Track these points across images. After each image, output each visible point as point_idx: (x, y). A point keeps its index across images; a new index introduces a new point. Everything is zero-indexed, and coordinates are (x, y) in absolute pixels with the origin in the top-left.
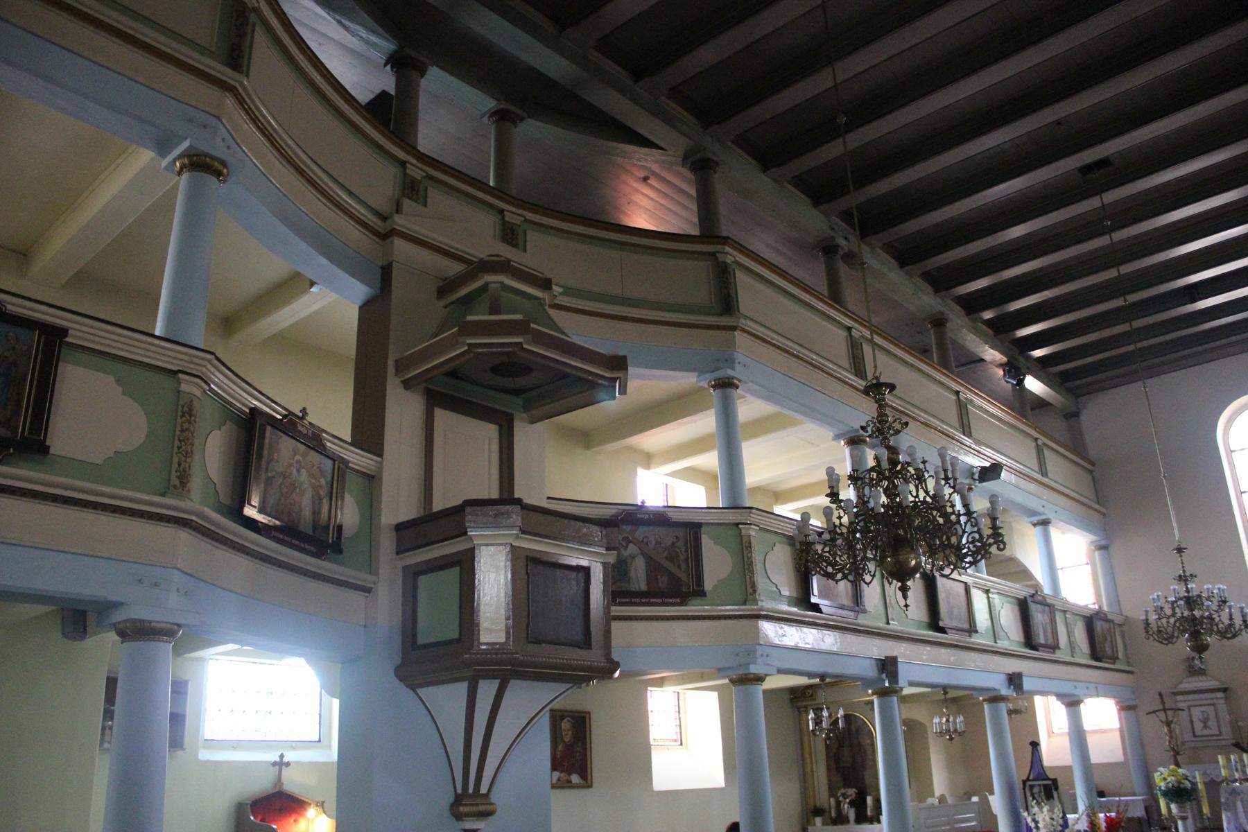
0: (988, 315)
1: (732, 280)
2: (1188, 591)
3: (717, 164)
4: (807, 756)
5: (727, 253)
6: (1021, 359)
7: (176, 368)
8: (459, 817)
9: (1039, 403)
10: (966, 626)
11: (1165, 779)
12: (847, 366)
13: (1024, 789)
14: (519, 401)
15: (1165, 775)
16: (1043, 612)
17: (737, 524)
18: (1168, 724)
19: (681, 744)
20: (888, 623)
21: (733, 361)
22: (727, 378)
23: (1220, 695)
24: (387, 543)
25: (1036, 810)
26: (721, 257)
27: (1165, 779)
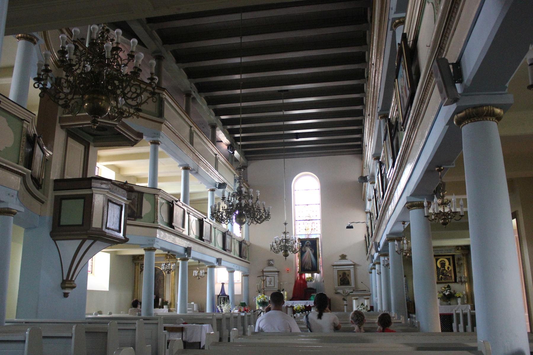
0: (229, 127)
1: (163, 105)
2: (286, 237)
3: (164, 58)
4: (136, 282)
5: (164, 94)
6: (235, 144)
7: (23, 118)
8: (63, 288)
9: (236, 160)
10: (209, 239)
11: (260, 299)
12: (189, 141)
13: (218, 298)
14: (92, 138)
15: (260, 297)
16: (229, 238)
17: (155, 194)
18: (264, 281)
19: (92, 273)
20: (189, 235)
21: (160, 135)
22: (157, 141)
23: (277, 273)
24: (51, 186)
25: (222, 305)
26: (161, 95)
27: (260, 299)
